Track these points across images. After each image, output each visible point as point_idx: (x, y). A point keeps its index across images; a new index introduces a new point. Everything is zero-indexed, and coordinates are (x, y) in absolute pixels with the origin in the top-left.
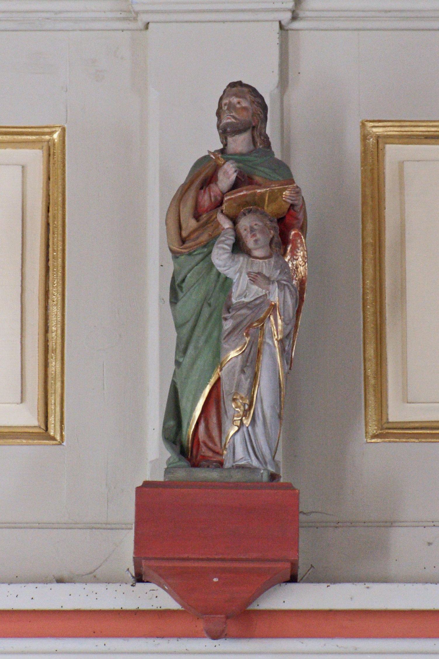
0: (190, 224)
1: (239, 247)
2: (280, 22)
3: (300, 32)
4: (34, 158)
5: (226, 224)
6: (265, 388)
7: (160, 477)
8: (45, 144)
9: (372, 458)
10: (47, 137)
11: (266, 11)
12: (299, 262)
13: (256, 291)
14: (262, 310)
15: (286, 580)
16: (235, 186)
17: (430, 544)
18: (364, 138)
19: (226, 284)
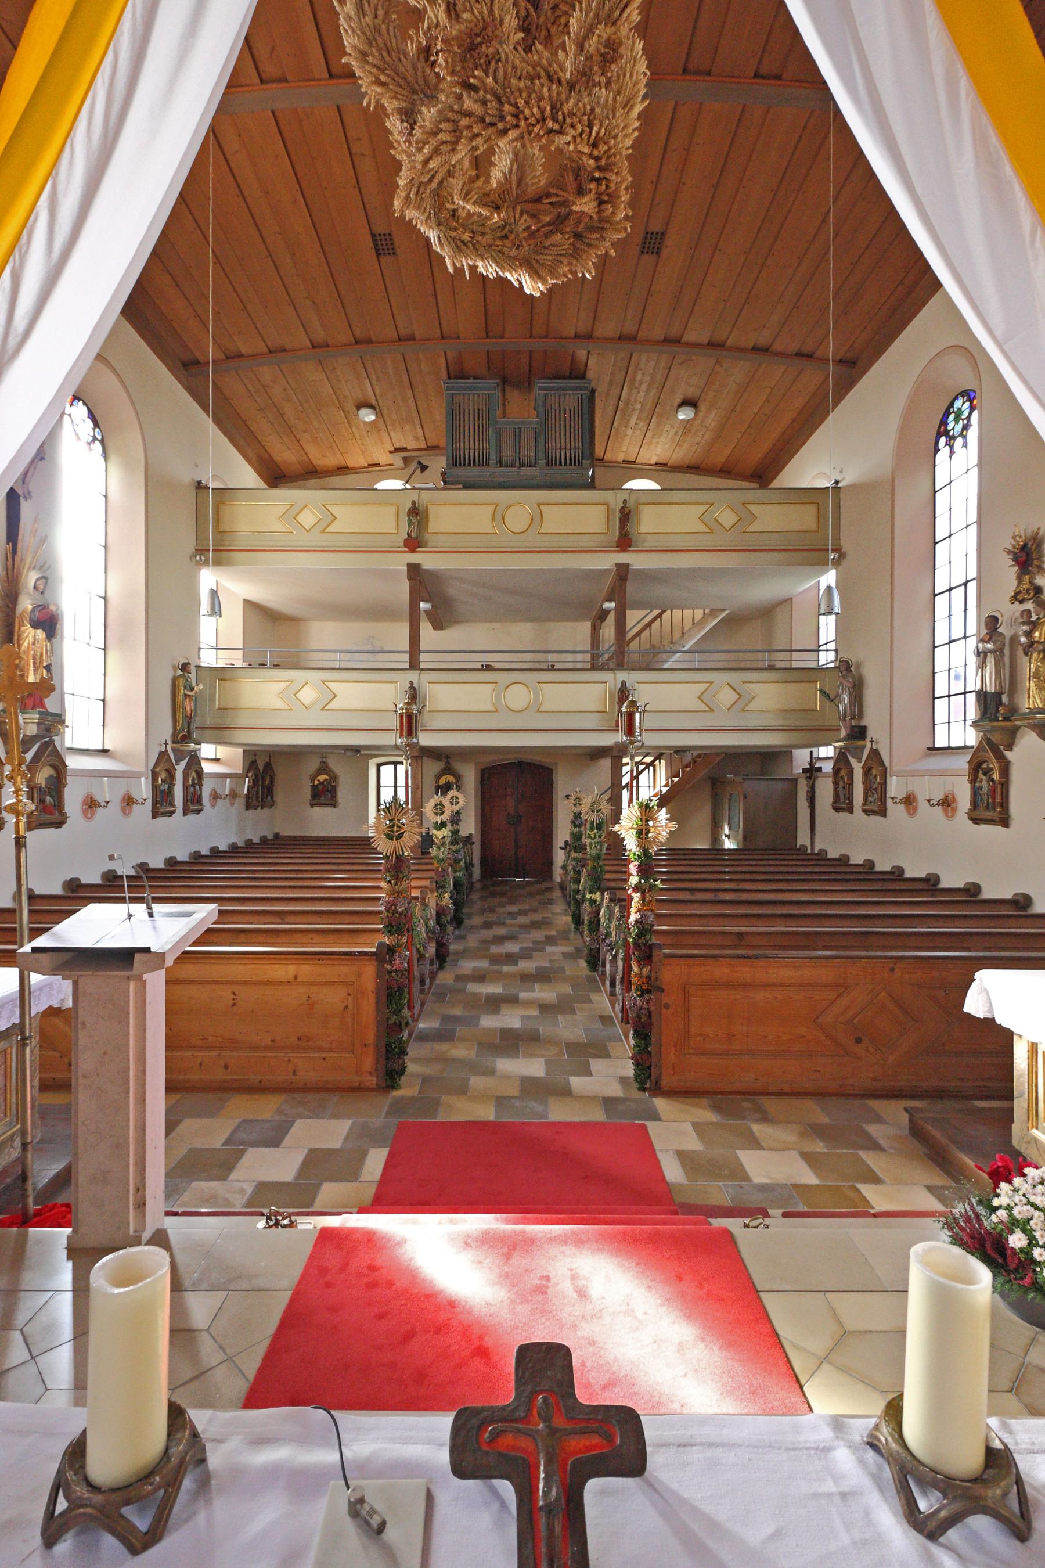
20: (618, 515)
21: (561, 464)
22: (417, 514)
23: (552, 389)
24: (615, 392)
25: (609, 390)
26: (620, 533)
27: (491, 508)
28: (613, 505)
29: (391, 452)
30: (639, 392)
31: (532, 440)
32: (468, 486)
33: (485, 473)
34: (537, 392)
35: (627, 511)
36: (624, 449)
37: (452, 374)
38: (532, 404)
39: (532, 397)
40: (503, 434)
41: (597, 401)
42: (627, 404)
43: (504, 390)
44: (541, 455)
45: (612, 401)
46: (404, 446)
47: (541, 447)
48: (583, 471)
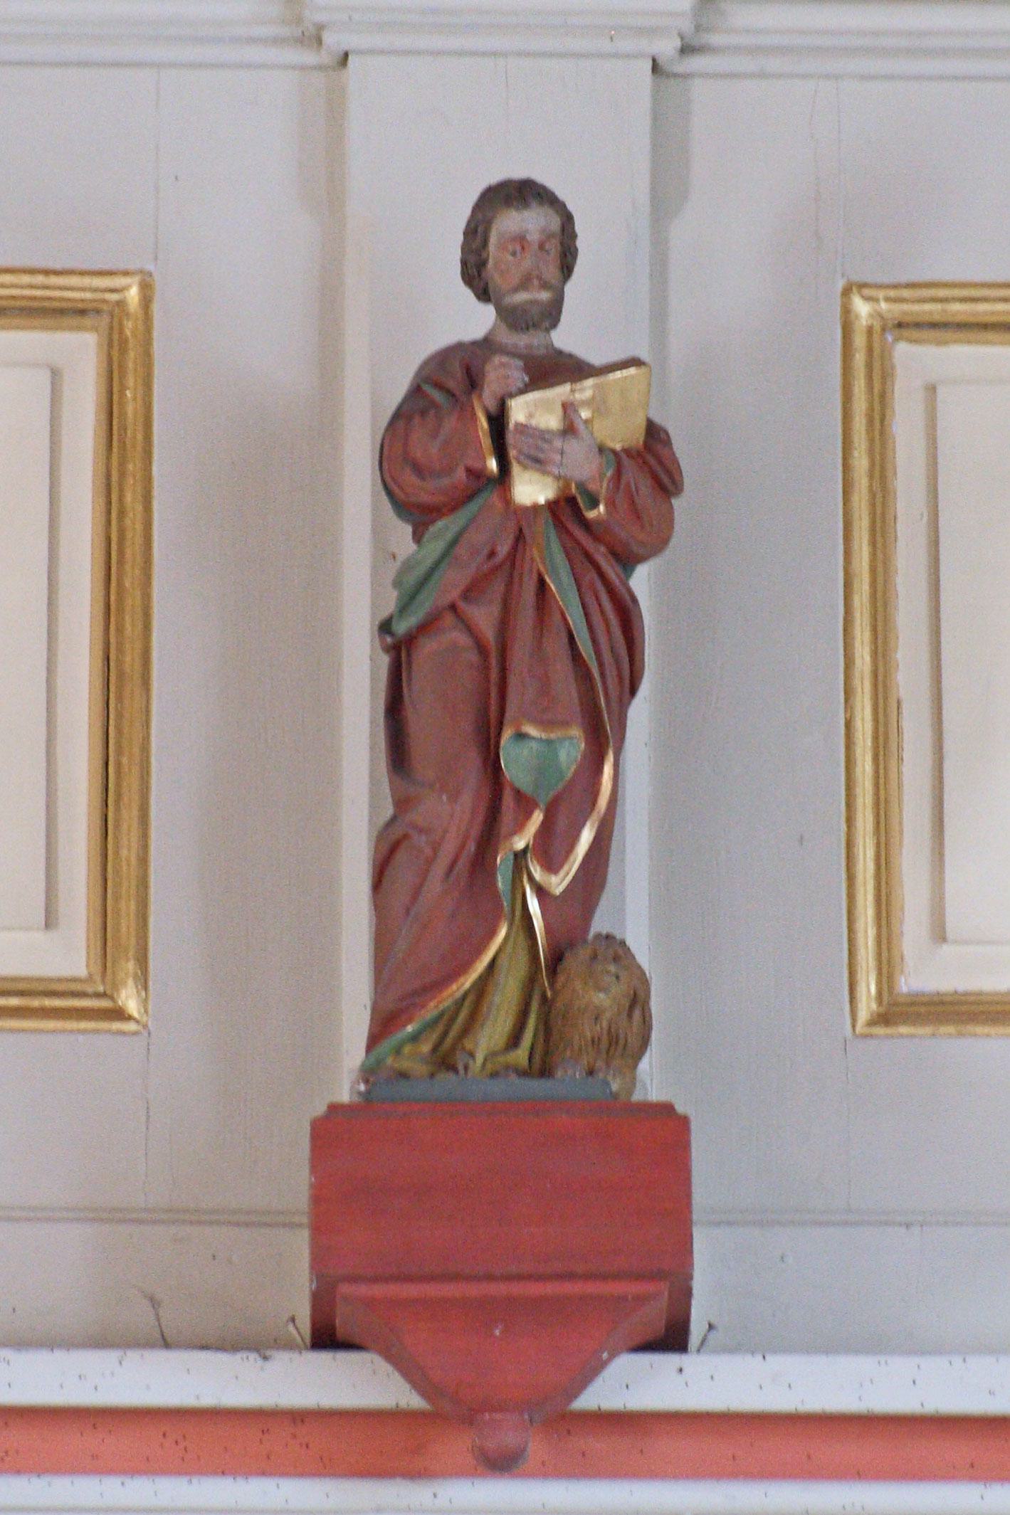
2: (654, 60)
3: (697, 81)
4: (80, 350)
8: (105, 320)
10: (114, 297)
11: (50, 584)
15: (649, 1336)
17: (435, 1496)
20: (362, 555)
35: (552, 443)
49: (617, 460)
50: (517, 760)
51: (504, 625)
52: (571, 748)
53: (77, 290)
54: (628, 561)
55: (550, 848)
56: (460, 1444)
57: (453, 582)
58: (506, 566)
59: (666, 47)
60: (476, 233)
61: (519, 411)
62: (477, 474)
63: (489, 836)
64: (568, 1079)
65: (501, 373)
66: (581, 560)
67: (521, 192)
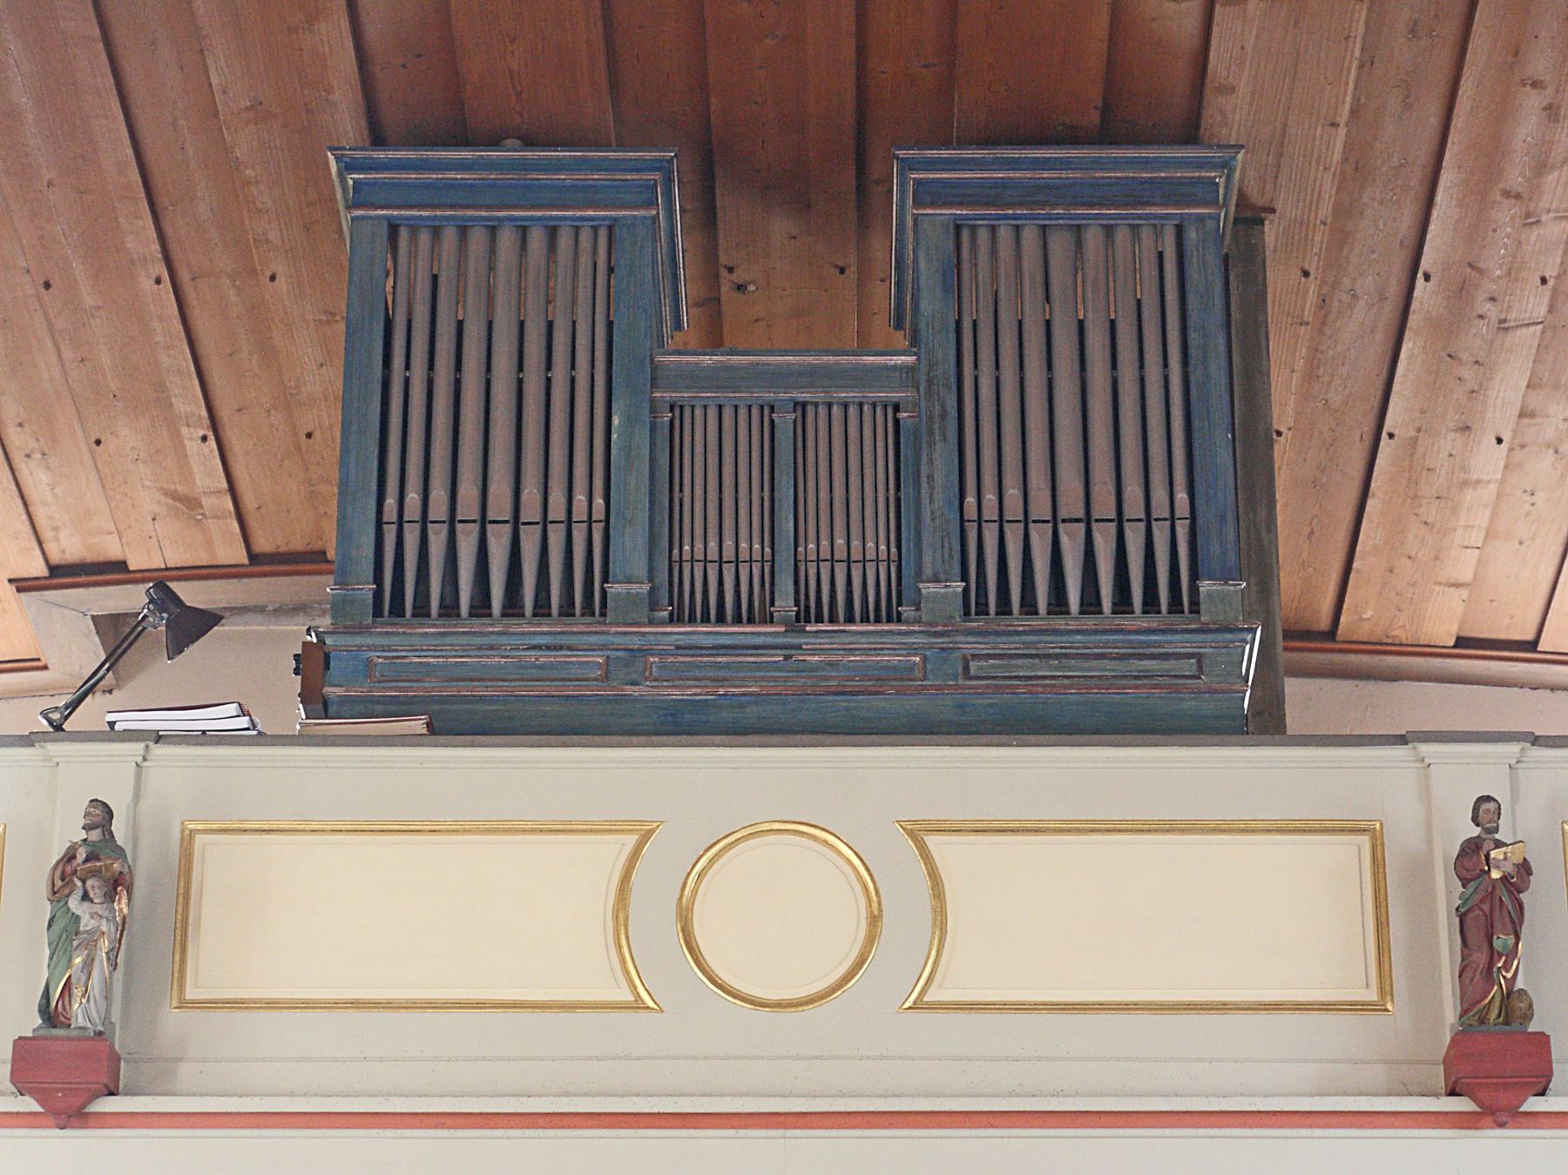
0: (59, 883)
1: (86, 897)
4: (1365, 840)
5: (79, 884)
6: (96, 982)
7: (30, 1035)
9: (172, 1019)
12: (122, 905)
13: (93, 923)
14: (95, 934)
16: (86, 860)
18: (183, 831)
19: (77, 919)
20: (1446, 893)
21: (1059, 602)
22: (117, 884)
23: (992, 195)
24: (1382, 224)
25: (1346, 211)
26: (1468, 1006)
27: (619, 847)
28: (1403, 836)
29: (23, 585)
30: (1530, 220)
31: (878, 469)
32: (455, 722)
33: (585, 650)
34: (914, 222)
35: (1501, 863)
36: (1463, 566)
37: (391, 117)
38: (882, 296)
39: (881, 253)
40: (700, 437)
41: (1279, 279)
42: (1460, 292)
43: (707, 216)
44: (934, 552)
45: (1371, 279)
46: (112, 549)
47: (936, 501)
48: (1205, 644)
49: (1518, 866)
50: (1497, 944)
51: (1492, 910)
52: (1511, 940)
53: (1364, 825)
54: (1520, 892)
55: (1507, 967)
56: (1489, 1120)
57: (1477, 898)
58: (1490, 895)
59: (1513, 761)
60: (1476, 810)
61: (1493, 854)
62: (1483, 871)
63: (1491, 964)
64: (1515, 1026)
65: (1488, 845)
66: (1510, 892)
67: (1489, 799)
